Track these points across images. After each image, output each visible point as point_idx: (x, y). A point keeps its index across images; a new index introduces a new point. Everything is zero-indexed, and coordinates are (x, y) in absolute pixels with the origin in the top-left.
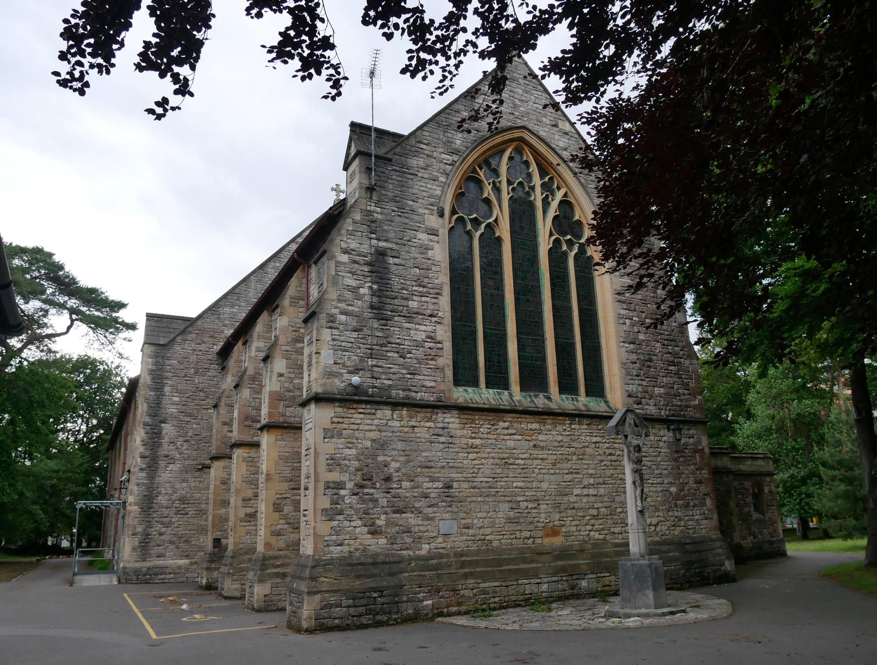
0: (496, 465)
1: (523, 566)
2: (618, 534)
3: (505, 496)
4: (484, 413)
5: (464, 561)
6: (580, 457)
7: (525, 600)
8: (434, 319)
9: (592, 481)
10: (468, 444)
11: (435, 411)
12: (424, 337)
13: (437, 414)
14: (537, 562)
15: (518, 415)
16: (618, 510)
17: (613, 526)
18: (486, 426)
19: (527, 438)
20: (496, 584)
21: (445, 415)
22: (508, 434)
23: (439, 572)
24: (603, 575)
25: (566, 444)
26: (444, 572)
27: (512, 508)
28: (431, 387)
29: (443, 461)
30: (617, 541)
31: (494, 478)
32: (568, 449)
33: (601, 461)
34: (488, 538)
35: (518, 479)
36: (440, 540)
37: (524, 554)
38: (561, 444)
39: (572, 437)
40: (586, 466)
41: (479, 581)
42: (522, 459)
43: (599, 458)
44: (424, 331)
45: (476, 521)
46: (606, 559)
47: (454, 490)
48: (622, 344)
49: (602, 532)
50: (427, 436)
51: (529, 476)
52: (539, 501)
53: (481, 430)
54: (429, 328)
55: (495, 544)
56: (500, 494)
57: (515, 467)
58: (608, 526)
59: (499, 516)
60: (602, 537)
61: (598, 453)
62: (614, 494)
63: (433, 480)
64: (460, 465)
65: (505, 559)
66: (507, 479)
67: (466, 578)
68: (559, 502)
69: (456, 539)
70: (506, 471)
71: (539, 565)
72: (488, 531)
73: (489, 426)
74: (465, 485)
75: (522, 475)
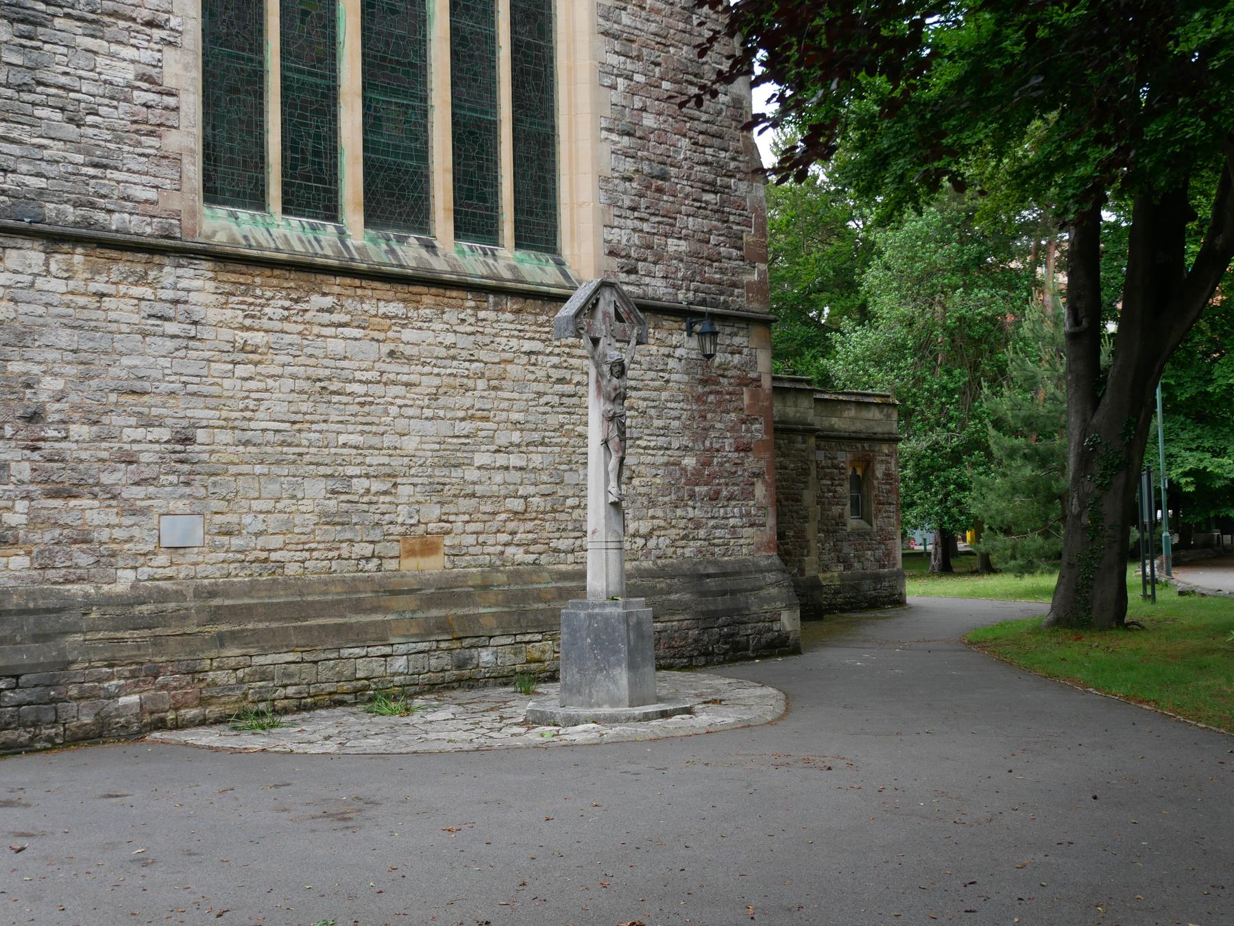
0: (302, 392)
1: (354, 619)
2: (566, 552)
3: (318, 464)
4: (277, 272)
5: (218, 607)
6: (493, 383)
7: (355, 692)
8: (157, 34)
9: (516, 437)
10: (234, 342)
11: (157, 259)
12: (131, 76)
13: (161, 266)
14: (386, 610)
15: (357, 282)
16: (570, 502)
17: (557, 535)
18: (280, 303)
19: (376, 335)
20: (290, 657)
21: (180, 271)
22: (332, 325)
23: (158, 631)
24: (528, 637)
25: (465, 354)
26: (169, 632)
27: (333, 492)
28: (146, 201)
29: (173, 378)
30: (563, 567)
31: (294, 423)
32: (467, 364)
33: (540, 394)
34: (274, 556)
35: (350, 428)
36: (162, 559)
37: (359, 592)
38: (452, 352)
39: (479, 337)
40: (505, 405)
41: (252, 651)
42: (360, 381)
43: (536, 387)
44: (133, 62)
45: (247, 519)
46: (536, 606)
47: (197, 448)
48: (604, 134)
49: (532, 548)
50: (135, 318)
51: (376, 420)
52: (396, 476)
53: (266, 310)
54: (146, 56)
55: (292, 569)
56: (307, 458)
57: (344, 399)
58: (545, 535)
59: (303, 509)
60: (532, 557)
61: (532, 377)
62: (563, 467)
63: (148, 423)
64: (215, 390)
65: (313, 602)
66: (324, 426)
67: (222, 645)
68: (442, 480)
69: (201, 559)
70: (322, 408)
71: (390, 617)
72: (277, 541)
73: (287, 304)
74: (225, 437)
75: (360, 419)
